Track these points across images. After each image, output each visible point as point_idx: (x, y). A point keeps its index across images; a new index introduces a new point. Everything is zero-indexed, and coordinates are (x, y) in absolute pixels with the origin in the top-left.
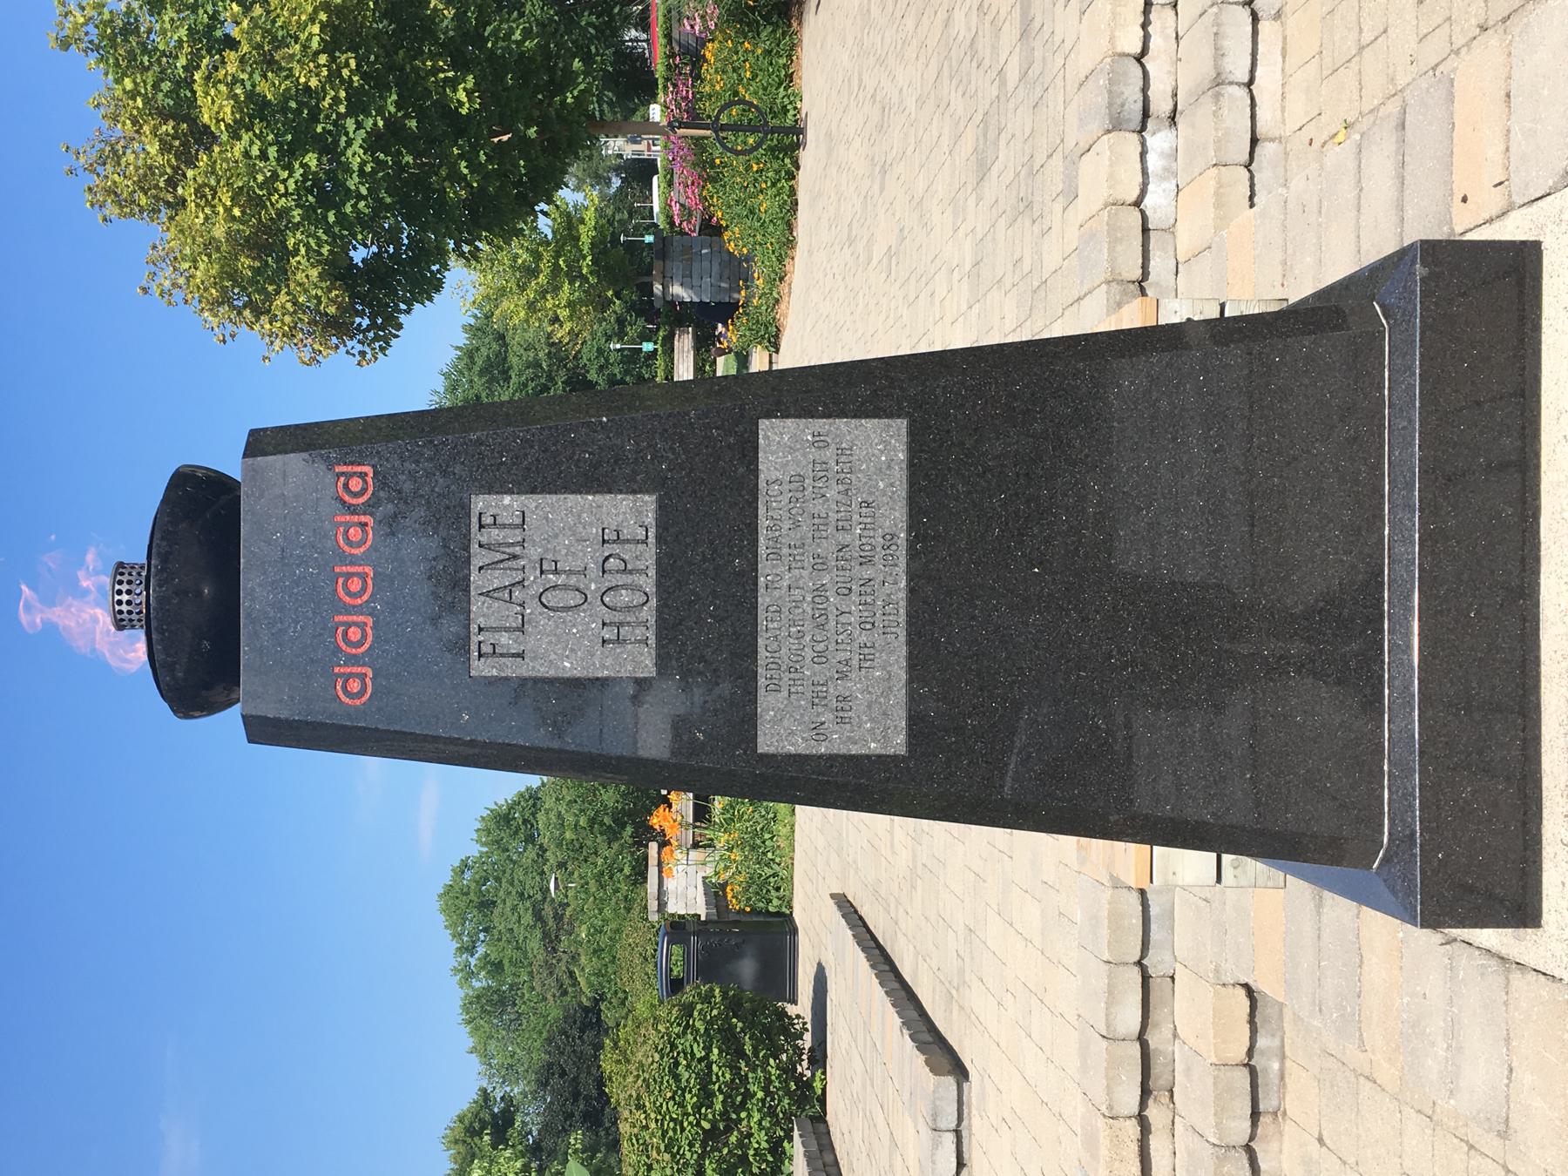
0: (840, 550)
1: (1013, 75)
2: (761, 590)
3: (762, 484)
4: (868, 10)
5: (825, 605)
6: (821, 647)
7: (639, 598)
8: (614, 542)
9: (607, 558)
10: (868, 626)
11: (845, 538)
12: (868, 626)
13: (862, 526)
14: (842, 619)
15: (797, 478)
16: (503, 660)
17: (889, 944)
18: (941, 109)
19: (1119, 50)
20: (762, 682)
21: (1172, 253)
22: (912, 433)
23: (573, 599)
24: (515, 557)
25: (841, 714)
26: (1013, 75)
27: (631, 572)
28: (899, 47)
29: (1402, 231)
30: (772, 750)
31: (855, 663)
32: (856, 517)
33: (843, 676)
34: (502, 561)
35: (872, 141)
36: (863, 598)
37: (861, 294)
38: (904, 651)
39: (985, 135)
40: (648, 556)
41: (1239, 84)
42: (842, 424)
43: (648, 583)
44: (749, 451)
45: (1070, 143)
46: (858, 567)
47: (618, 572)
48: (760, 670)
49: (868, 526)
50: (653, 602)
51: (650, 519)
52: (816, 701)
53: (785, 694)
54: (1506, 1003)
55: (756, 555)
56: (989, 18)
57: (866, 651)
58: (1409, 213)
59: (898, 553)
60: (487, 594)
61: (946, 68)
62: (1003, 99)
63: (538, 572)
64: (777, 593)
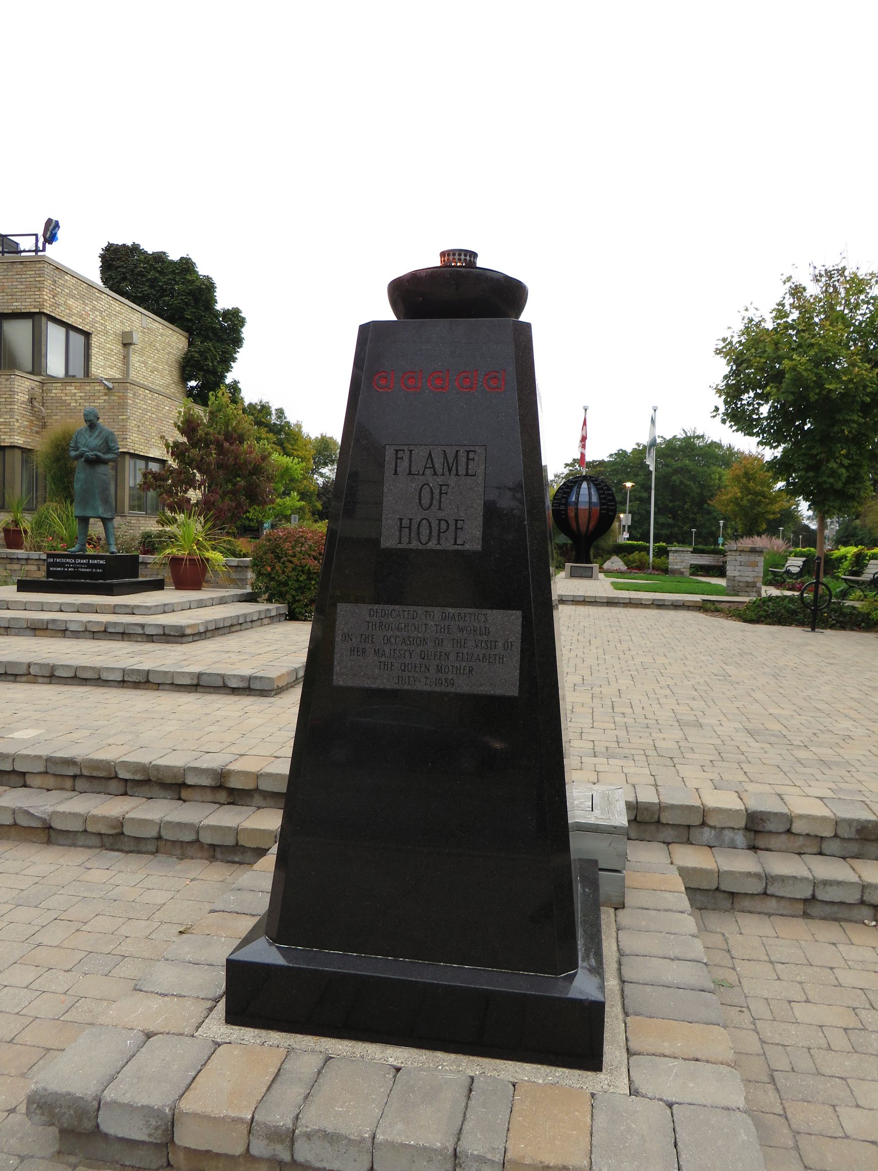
0: (446, 654)
1: (802, 754)
2: (426, 609)
3: (484, 611)
4: (871, 671)
5: (415, 643)
6: (393, 640)
7: (423, 541)
8: (456, 526)
9: (447, 522)
10: (403, 668)
11: (452, 657)
12: (403, 668)
13: (459, 667)
14: (407, 654)
15: (487, 631)
16: (394, 462)
17: (290, 665)
18: (798, 710)
19: (794, 820)
20: (376, 607)
21: (676, 841)
22: (510, 698)
23: (426, 501)
24: (450, 470)
25: (356, 650)
26: (802, 754)
27: (439, 535)
28: (844, 687)
29: (639, 983)
30: (338, 611)
31: (383, 659)
32: (464, 664)
33: (376, 652)
34: (448, 463)
35: (795, 669)
36: (418, 666)
37: (710, 658)
38: (389, 687)
39: (773, 735)
40: (447, 545)
41: (766, 888)
42: (517, 657)
43: (432, 545)
44: (505, 605)
45: (750, 787)
46: (436, 663)
47: (439, 528)
48: (381, 606)
49: (458, 671)
50: (421, 547)
51: (467, 547)
52: (439, 628)
53: (368, 619)
54: (198, 997)
55: (445, 606)
56: (841, 743)
57: (389, 666)
58: (648, 989)
59: (443, 686)
60: (430, 455)
61: (822, 715)
62: (789, 747)
63: (441, 483)
64: (424, 617)
